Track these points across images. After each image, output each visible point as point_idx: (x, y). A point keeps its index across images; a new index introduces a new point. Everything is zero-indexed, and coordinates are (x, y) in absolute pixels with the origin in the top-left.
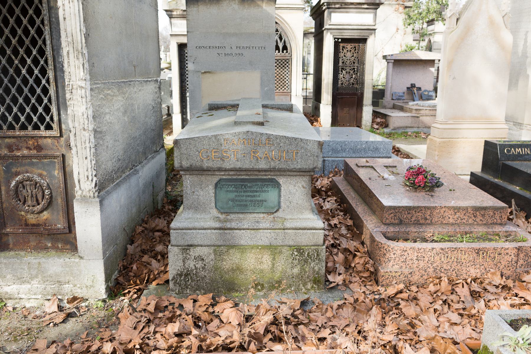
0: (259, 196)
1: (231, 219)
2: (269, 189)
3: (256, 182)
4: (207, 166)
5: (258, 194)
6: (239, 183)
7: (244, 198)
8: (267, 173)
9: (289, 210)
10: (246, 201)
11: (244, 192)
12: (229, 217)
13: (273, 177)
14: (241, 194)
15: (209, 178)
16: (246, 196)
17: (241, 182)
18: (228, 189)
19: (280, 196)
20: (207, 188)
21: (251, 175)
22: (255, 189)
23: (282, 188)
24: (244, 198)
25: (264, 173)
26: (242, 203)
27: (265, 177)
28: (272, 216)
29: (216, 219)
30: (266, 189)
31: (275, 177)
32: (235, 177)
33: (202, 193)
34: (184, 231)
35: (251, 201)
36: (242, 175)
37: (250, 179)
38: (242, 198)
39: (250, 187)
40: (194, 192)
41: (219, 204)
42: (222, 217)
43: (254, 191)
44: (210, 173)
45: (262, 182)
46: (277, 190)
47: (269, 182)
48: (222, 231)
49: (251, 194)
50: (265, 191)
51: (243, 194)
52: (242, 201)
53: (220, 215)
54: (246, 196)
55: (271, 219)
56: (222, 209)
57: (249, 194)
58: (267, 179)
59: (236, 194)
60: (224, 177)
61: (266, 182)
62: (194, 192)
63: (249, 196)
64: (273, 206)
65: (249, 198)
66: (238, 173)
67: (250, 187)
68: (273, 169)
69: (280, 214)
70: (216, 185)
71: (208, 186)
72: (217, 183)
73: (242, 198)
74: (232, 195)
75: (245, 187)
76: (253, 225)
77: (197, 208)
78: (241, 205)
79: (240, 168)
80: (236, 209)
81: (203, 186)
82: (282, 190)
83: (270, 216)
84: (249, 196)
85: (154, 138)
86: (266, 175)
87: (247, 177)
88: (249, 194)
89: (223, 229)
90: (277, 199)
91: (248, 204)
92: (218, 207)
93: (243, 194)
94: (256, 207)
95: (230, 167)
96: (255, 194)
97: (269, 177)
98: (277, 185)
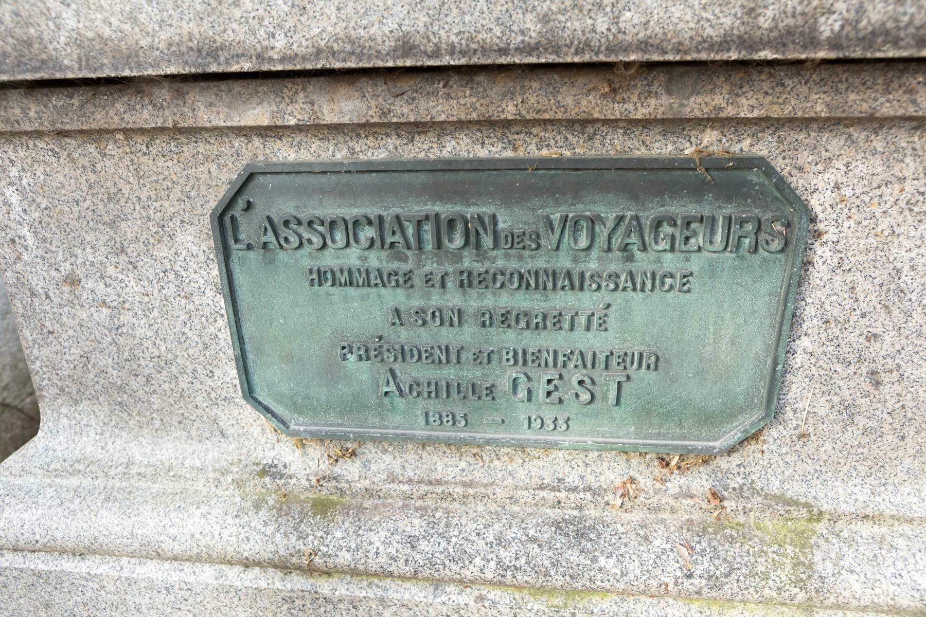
0: (598, 322)
1: (369, 493)
2: (696, 264)
3: (577, 191)
4: (78, 42)
5: (587, 301)
6: (418, 208)
7: (468, 334)
8: (696, 105)
9: (851, 436)
10: (484, 358)
11: (467, 281)
12: (350, 470)
13: (744, 146)
14: (436, 299)
15: (161, 161)
16: (487, 320)
17: (438, 193)
18: (328, 260)
19: (788, 322)
20: (162, 252)
21: (523, 124)
22: (564, 262)
23: (822, 253)
24: (468, 334)
25: (659, 104)
26: (449, 373)
27: (662, 148)
28: (700, 481)
29: (255, 487)
30: (670, 262)
31: (762, 146)
32: (378, 151)
33: (133, 288)
34: (39, 563)
35: (522, 358)
36: (440, 128)
37: (516, 166)
38: (447, 335)
39: (515, 240)
40: (73, 281)
41: (270, 376)
42: (303, 463)
43: (549, 280)
44: (145, 115)
45: (634, 194)
46: (773, 280)
47: (698, 191)
48: (298, 582)
49: (522, 301)
50: (657, 280)
51: (453, 298)
52: (452, 355)
53: (286, 453)
54: (487, 320)
55: (694, 511)
56: (298, 409)
57: (505, 300)
58: (686, 165)
59: (394, 297)
60: (285, 152)
61: (673, 190)
62: (73, 281)
63: (505, 319)
64: (714, 404)
65: (510, 339)
66: (402, 111)
67: (515, 240)
68: (783, 38)
69: (772, 465)
70: (224, 223)
71: (164, 232)
72: (230, 204)
73: (447, 335)
74: (364, 312)
75: (472, 240)
76: (543, 558)
77: (129, 391)
78: (437, 390)
79: (406, 46)
80: (408, 416)
81: (129, 229)
82: (819, 273)
83: (677, 482)
84: (505, 319)
85: (517, 202)
86: (675, 125)
87: (491, 149)
88: (505, 300)
89: (310, 570)
90: (758, 344)
91: (504, 384)
92: (262, 395)
93: (453, 298)
94: (572, 408)
95: (301, 44)
96: (563, 300)
97: (710, 140)
98: (775, 221)
